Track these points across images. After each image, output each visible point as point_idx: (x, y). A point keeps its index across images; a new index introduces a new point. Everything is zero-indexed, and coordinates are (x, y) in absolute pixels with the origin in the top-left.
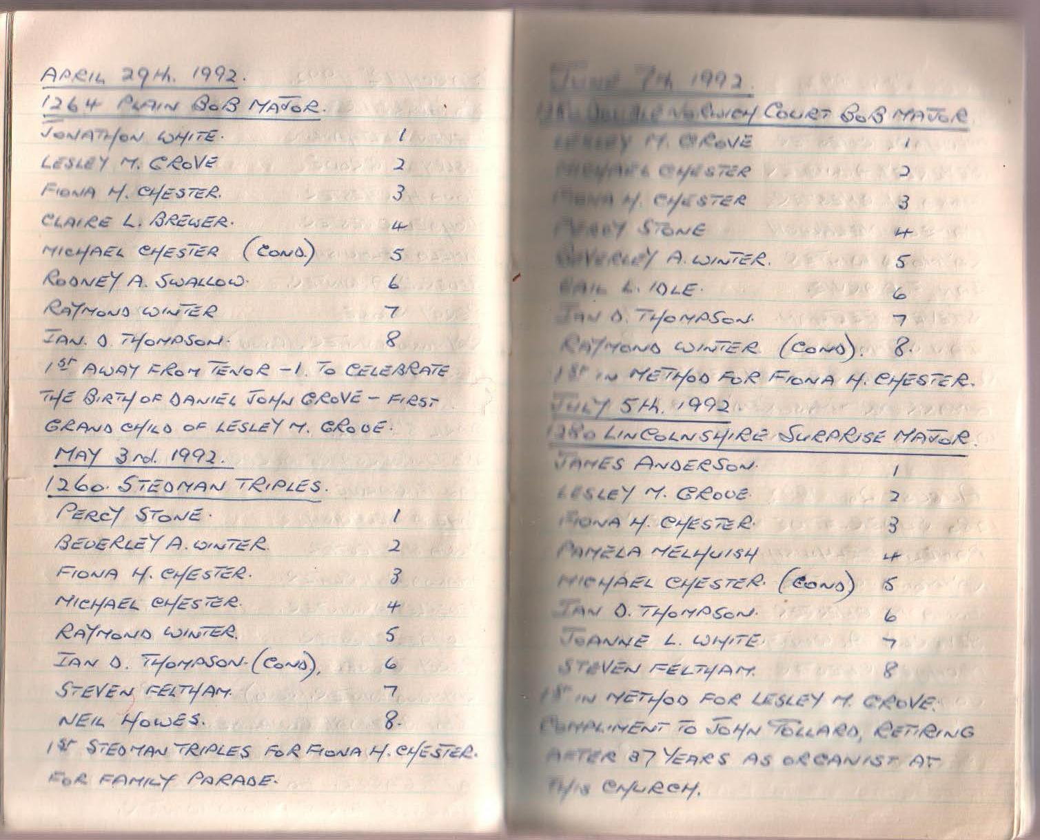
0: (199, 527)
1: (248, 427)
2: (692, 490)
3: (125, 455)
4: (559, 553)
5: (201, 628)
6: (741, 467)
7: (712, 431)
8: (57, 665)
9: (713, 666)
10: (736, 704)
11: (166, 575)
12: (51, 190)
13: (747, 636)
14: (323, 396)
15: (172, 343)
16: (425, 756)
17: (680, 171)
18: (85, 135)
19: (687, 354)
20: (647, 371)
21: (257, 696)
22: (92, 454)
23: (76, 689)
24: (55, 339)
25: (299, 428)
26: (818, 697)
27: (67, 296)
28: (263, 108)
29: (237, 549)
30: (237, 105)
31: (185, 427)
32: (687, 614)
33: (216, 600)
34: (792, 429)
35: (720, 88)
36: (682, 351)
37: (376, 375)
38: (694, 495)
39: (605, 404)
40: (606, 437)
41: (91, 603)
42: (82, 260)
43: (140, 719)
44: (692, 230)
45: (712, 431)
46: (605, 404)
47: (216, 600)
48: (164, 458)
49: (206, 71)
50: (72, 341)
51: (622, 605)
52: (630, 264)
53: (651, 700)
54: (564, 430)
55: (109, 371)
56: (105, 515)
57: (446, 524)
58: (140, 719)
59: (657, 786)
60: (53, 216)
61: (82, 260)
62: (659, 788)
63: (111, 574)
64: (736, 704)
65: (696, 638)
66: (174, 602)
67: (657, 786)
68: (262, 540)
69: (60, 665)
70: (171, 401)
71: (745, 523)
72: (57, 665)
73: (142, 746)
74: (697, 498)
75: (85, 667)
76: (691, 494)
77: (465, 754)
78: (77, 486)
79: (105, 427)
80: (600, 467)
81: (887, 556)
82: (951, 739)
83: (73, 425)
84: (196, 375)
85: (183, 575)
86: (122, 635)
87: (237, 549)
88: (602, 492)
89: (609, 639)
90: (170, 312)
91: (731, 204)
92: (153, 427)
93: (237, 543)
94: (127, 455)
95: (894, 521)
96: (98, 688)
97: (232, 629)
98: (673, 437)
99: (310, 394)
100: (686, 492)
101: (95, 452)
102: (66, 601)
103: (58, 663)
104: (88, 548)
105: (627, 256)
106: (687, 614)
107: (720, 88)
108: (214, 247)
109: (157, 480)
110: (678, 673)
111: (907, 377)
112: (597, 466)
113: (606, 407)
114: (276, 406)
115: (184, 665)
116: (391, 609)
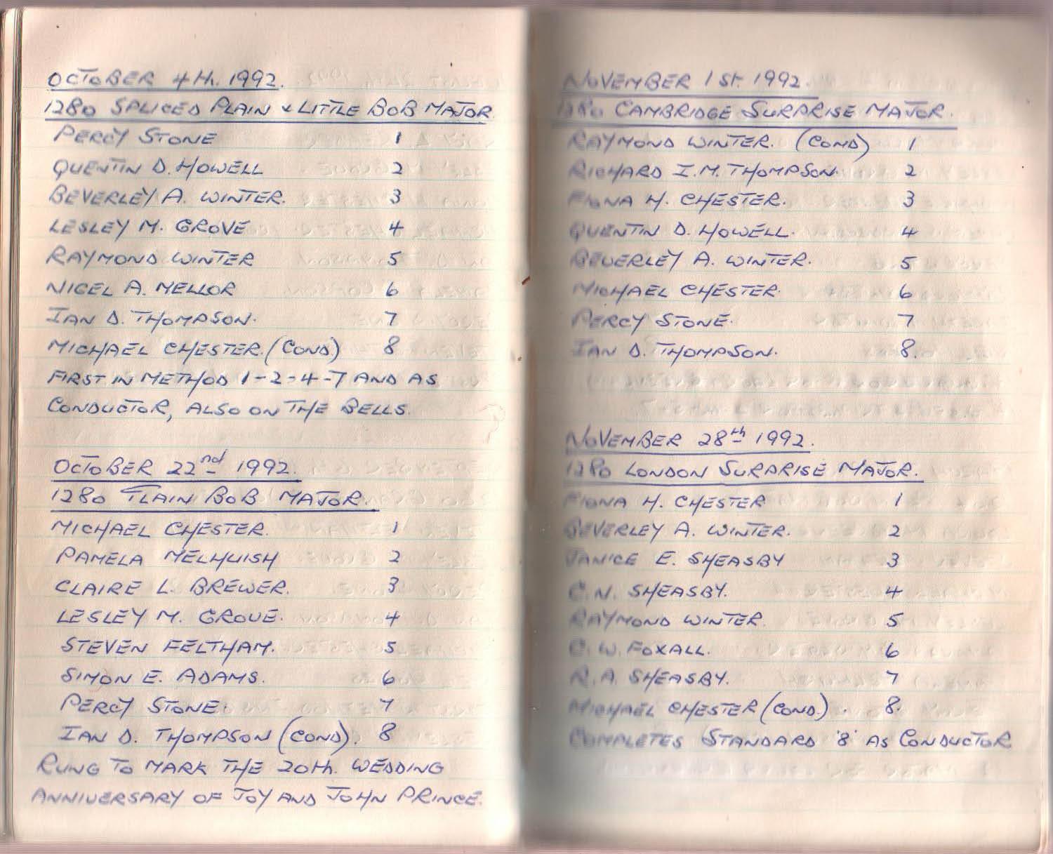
1: (101, 617)
3: (911, 198)
6: (256, 739)
7: (702, 553)
8: (62, 738)
10: (755, 624)
11: (686, 200)
12: (636, 649)
13: (743, 166)
14: (785, 467)
17: (611, 709)
22: (263, 795)
23: (230, 526)
26: (266, 793)
27: (77, 305)
28: (293, 500)
33: (755, 197)
34: (754, 107)
37: (635, 535)
42: (649, 601)
44: (713, 321)
45: (702, 553)
47: (755, 197)
52: (635, 745)
55: (738, 262)
57: (463, 497)
58: (713, 199)
61: (649, 601)
64: (755, 624)
70: (675, 232)
72: (62, 738)
73: (708, 350)
75: (772, 537)
81: (704, 290)
83: (283, 589)
90: (755, 261)
92: (229, 555)
98: (700, 651)
101: (266, 793)
102: (656, 529)
105: (630, 738)
108: (638, 255)
109: (233, 581)
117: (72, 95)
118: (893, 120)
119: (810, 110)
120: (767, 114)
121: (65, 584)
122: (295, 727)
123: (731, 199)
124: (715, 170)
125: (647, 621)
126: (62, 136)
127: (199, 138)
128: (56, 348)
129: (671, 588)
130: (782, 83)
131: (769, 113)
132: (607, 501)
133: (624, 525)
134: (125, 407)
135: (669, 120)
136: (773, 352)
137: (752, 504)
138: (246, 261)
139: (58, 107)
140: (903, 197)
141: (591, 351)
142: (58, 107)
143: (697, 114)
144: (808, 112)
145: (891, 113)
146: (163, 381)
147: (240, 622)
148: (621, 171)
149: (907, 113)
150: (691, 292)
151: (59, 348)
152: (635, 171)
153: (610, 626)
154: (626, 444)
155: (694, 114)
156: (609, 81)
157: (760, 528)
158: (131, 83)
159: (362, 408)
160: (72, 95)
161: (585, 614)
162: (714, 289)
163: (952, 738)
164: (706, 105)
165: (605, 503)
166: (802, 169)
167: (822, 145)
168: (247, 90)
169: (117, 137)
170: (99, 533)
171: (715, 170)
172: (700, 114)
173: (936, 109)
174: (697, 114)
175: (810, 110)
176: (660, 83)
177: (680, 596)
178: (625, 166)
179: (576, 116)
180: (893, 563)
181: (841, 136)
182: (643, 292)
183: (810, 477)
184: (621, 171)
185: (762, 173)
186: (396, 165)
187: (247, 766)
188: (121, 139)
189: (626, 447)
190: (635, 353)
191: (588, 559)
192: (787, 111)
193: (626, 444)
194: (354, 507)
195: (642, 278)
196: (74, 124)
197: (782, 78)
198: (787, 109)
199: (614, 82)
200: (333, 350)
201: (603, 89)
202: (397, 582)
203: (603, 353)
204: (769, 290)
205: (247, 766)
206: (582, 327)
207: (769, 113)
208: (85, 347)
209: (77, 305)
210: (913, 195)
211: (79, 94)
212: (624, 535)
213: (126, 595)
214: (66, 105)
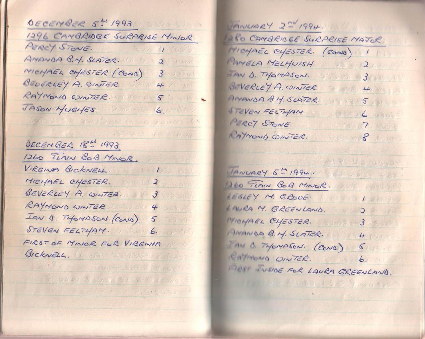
0: (107, 223)
2: (277, 207)
4: (231, 123)
9: (42, 217)
15: (283, 247)
18: (253, 51)
20: (112, 156)
24: (32, 217)
25: (167, 37)
36: (74, 99)
38: (278, 210)
39: (54, 47)
40: (57, 159)
46: (54, 47)
50: (39, 218)
51: (52, 216)
53: (267, 246)
54: (232, 184)
60: (48, 22)
66: (72, 218)
69: (29, 218)
70: (50, 219)
71: (307, 221)
74: (279, 211)
76: (277, 209)
77: (262, 27)
80: (246, 65)
84: (82, 220)
85: (281, 222)
86: (78, 218)
88: (245, 196)
89: (40, 217)
91: (249, 89)
97: (319, 233)
100: (275, 208)
103: (28, 218)
111: (276, 62)
112: (245, 64)
113: (54, 48)
114: (79, 184)
117: (38, 31)
118: (361, 43)
119: (328, 39)
120: (310, 40)
122: (117, 216)
123: (88, 72)
124: (272, 196)
125: (298, 247)
126: (324, 40)
128: (70, 244)
129: (315, 233)
130: (310, 28)
131: (311, 40)
136: (303, 247)
138: (315, 101)
140: (158, 72)
141: (34, 218)
142: (30, 157)
143: (283, 40)
144: (328, 39)
145: (360, 40)
149: (366, 41)
153: (247, 224)
154: (49, 146)
155: (282, 39)
157: (307, 86)
158: (75, 26)
160: (38, 31)
162: (283, 221)
164: (288, 36)
166: (289, 245)
169: (50, 48)
171: (272, 196)
172: (285, 40)
173: (378, 39)
174: (283, 40)
175: (328, 39)
177: (305, 236)
179: (234, 41)
180: (161, 75)
181: (341, 49)
182: (254, 221)
185: (274, 76)
186: (113, 76)
188: (52, 49)
190: (51, 218)
192: (331, 39)
193: (49, 146)
194: (70, 149)
196: (33, 42)
197: (39, 35)
198: (319, 38)
200: (140, 74)
202: (132, 221)
203: (236, 233)
206: (234, 124)
207: (311, 40)
208: (39, 254)
211: (40, 31)
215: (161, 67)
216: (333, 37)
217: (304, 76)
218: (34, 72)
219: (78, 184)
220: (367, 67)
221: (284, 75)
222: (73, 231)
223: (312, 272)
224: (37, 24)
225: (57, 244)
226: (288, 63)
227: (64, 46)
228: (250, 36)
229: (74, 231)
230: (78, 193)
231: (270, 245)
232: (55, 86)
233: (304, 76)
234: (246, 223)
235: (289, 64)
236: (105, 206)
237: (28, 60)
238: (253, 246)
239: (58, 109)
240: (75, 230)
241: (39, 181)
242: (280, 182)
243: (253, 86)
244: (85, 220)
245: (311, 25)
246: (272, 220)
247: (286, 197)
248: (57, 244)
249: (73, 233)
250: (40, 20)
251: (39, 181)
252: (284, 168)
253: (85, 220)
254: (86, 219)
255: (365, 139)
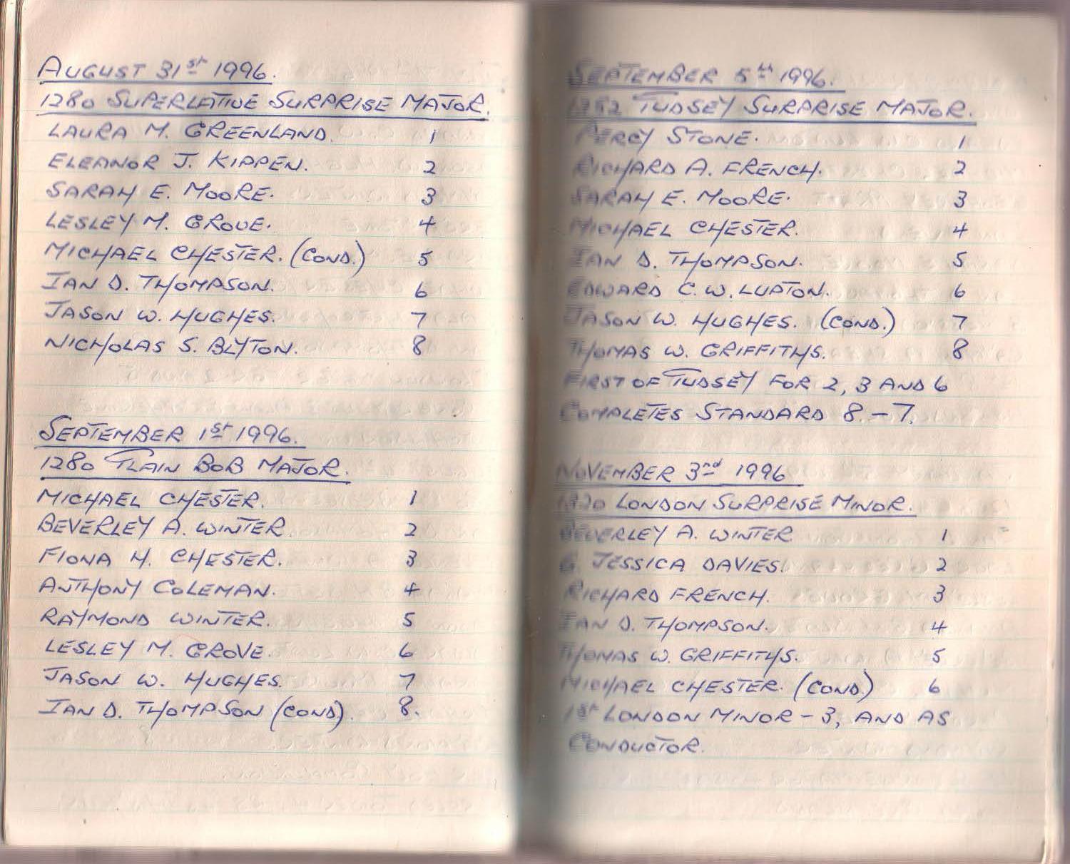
3: (941, 593)
5: (713, 473)
16: (767, 539)
19: (199, 323)
21: (798, 743)
27: (84, 271)
29: (747, 691)
30: (832, 715)
31: (158, 158)
32: (722, 262)
35: (591, 479)
37: (633, 539)
41: (709, 227)
43: (725, 228)
48: (187, 471)
49: (767, 469)
56: (740, 594)
59: (693, 743)
62: (694, 745)
63: (724, 565)
65: (652, 656)
67: (693, 743)
68: (272, 251)
78: (732, 324)
79: (699, 380)
82: (753, 632)
85: (697, 262)
87: (747, 691)
93: (747, 684)
94: (944, 593)
95: (413, 554)
96: (160, 281)
99: (714, 345)
104: (200, 531)
105: (600, 286)
106: (722, 262)
107: (591, 479)
110: (656, 233)
115: (57, 251)
116: (408, 593)
121: (679, 684)
122: (309, 245)
123: (227, 558)
124: (165, 647)
127: (207, 316)
132: (613, 261)
133: (620, 530)
134: (653, 746)
135: (668, 512)
137: (133, 439)
139: (56, 100)
140: (403, 552)
146: (203, 592)
147: (771, 267)
148: (614, 686)
150: (702, 229)
151: (57, 251)
152: (632, 290)
154: (617, 475)
156: (595, 471)
159: (708, 595)
160: (73, 88)
161: (582, 585)
163: (634, 744)
165: (611, 263)
167: (298, 714)
168: (129, 648)
170: (89, 503)
171: (165, 647)
176: (642, 473)
178: (618, 680)
183: (807, 512)
184: (614, 686)
187: (723, 227)
189: (617, 479)
191: (586, 624)
193: (617, 475)
195: (627, 673)
199: (602, 471)
200: (865, 687)
201: (589, 479)
204: (768, 684)
205: (723, 227)
209: (84, 271)
210: (148, 321)
212: (623, 540)
213: (705, 601)
214: (66, 98)
215: (412, 544)
216: (770, 466)
217: (755, 627)
218: (76, 251)
219: (233, 321)
220: (962, 173)
221: (703, 627)
222: (652, 229)
223: (60, 135)
224: (83, 164)
225: (236, 685)
226: (686, 260)
227: (678, 132)
228: (273, 424)
229: (861, 109)
230: (186, 319)
231: (667, 623)
232: (95, 228)
233: (755, 627)
234: (610, 599)
235: (242, 684)
236: (809, 381)
237: (71, 194)
238: (625, 624)
239: (93, 344)
240: (660, 228)
241: (79, 497)
242: (44, 519)
243: (277, 525)
244: (770, 294)
245: (247, 67)
246: (696, 226)
247: (719, 351)
248: (236, 685)
249: (734, 387)
250: (86, 215)
251: (79, 497)
252: (766, 66)
253: (770, 294)
254: (772, 291)
255: (852, 415)
